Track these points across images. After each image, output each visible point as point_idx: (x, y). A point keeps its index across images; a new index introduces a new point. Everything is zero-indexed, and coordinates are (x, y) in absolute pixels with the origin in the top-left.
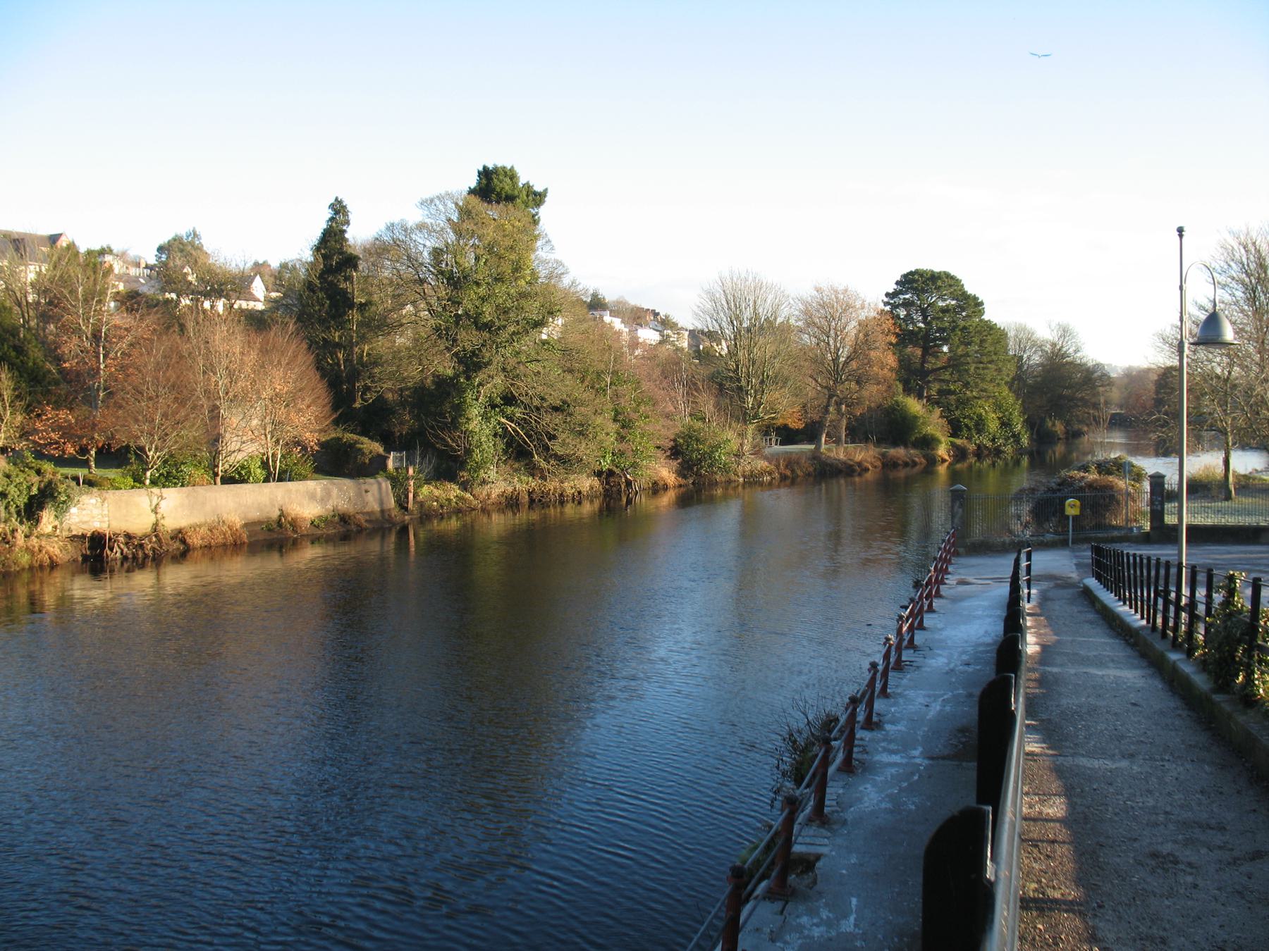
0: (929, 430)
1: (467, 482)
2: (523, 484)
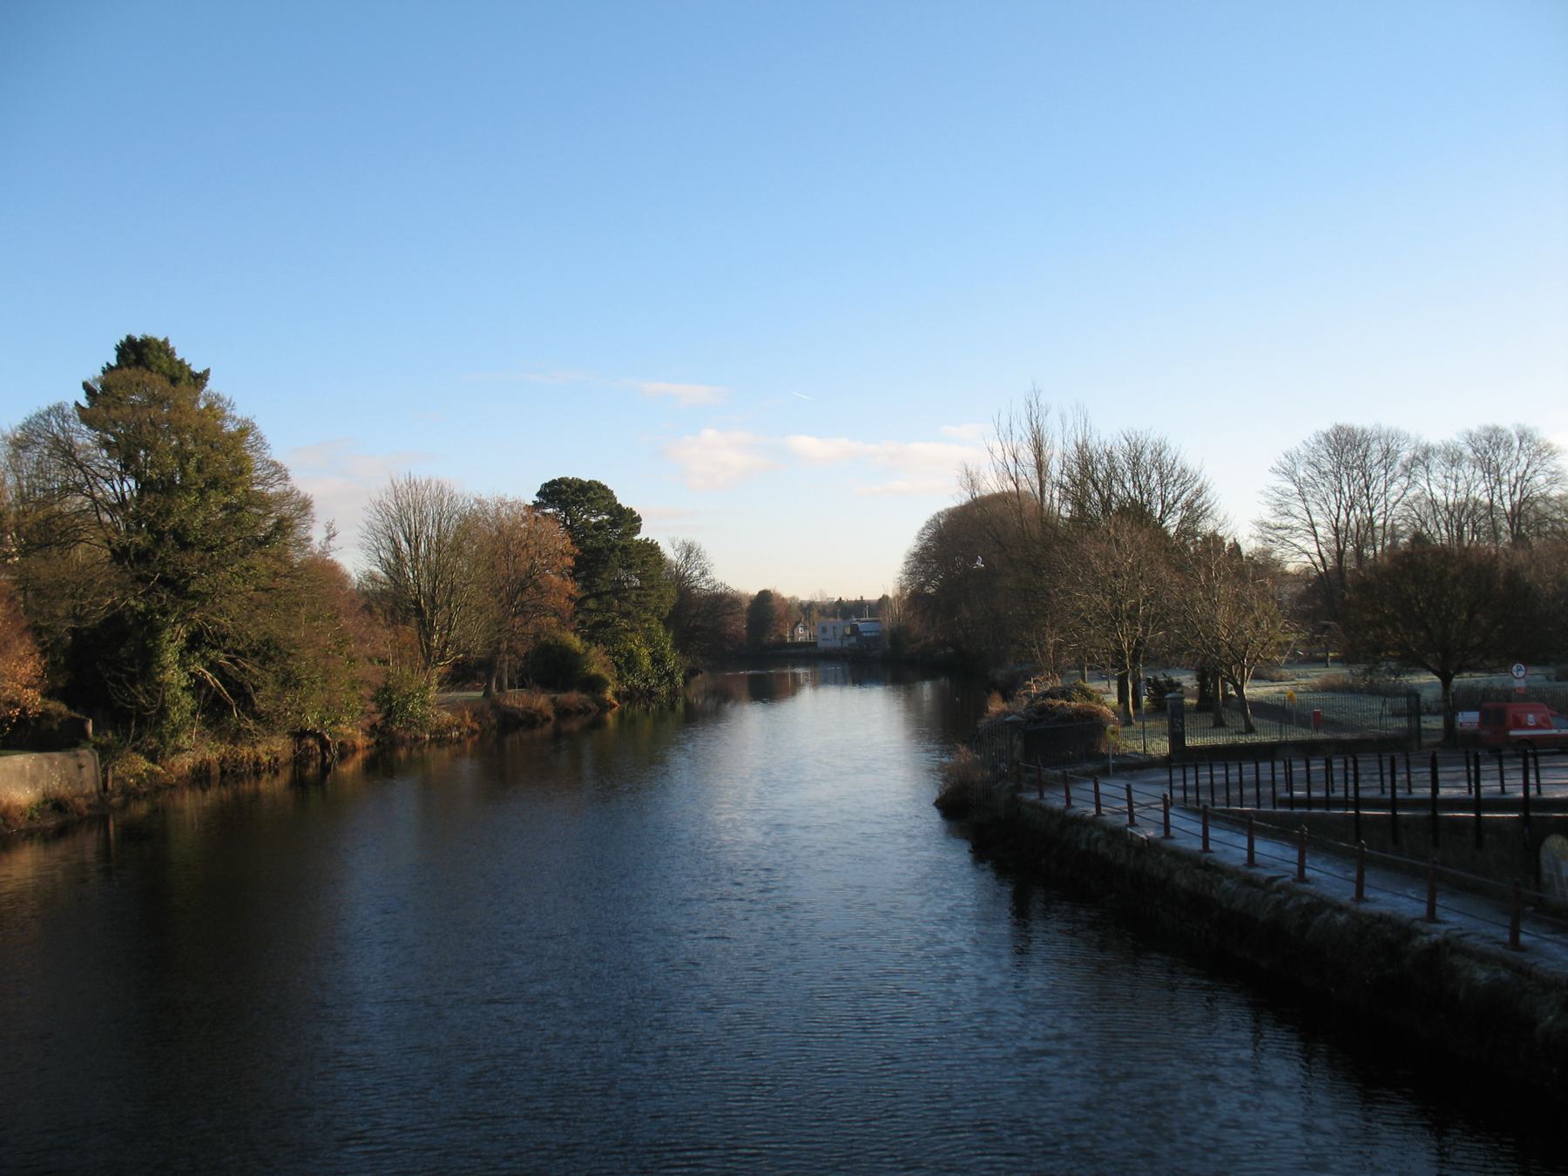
0: (595, 669)
1: (156, 750)
2: (213, 752)
